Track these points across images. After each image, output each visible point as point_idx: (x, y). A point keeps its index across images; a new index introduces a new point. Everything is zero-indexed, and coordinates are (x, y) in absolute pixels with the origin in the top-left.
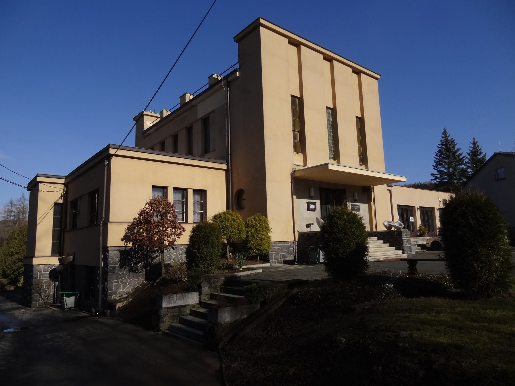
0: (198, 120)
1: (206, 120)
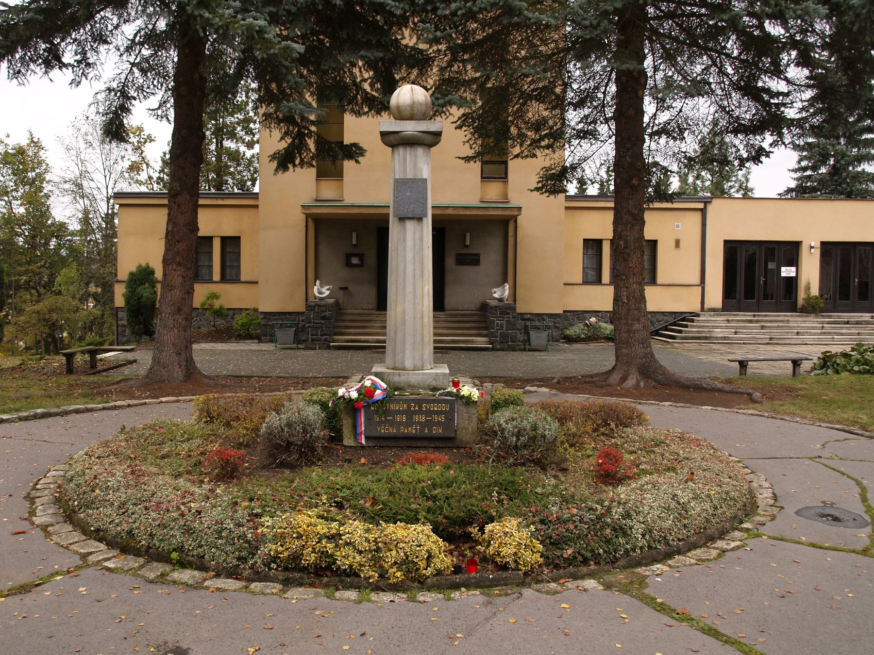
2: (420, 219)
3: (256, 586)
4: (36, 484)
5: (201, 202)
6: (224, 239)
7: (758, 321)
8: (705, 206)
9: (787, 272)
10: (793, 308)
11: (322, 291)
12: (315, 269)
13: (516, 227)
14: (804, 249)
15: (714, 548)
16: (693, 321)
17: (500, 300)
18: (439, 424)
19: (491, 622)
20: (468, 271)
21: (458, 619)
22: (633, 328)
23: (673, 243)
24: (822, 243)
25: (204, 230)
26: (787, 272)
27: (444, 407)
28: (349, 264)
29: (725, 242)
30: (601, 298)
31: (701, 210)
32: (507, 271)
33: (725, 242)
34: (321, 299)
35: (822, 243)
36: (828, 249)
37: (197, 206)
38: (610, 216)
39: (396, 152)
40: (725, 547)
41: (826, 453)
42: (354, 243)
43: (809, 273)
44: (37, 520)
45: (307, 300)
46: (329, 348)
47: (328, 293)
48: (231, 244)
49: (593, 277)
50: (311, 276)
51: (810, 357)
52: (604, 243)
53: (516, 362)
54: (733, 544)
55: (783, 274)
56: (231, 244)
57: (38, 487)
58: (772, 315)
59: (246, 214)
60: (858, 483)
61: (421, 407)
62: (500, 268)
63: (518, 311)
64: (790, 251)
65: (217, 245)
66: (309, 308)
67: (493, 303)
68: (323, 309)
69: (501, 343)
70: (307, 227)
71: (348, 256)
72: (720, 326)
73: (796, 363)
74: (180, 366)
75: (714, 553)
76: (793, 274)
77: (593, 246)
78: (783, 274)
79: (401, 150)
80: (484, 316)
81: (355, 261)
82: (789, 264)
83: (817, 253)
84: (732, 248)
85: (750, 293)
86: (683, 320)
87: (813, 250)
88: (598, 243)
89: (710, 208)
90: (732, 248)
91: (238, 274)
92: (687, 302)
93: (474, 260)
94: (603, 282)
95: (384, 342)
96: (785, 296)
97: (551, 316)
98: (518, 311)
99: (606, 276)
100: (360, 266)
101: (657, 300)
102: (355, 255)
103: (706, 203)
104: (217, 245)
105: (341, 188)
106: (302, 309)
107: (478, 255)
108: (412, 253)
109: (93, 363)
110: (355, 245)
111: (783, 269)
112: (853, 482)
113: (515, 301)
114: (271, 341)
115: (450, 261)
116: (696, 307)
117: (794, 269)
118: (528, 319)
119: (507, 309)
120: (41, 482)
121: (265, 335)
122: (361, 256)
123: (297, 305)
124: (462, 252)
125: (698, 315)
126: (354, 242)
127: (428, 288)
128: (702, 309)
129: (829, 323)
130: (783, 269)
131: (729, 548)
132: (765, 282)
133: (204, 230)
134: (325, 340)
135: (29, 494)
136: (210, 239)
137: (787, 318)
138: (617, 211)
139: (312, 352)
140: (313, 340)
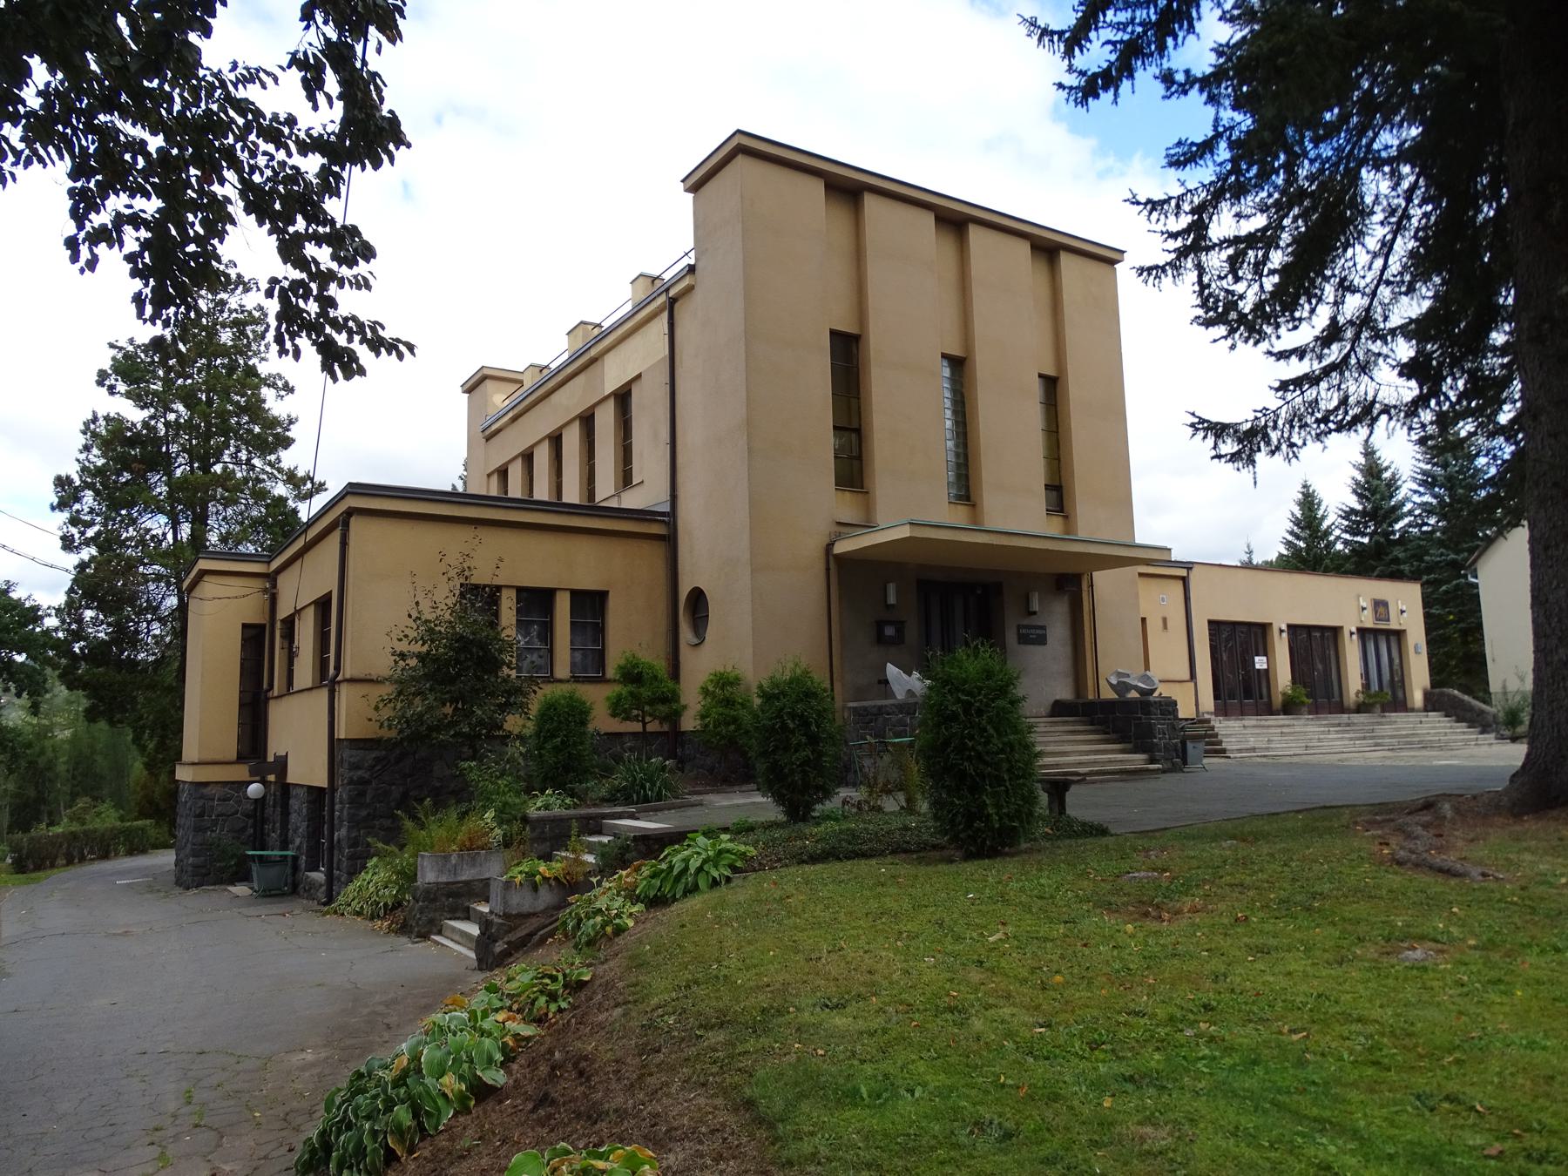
0: (515, 458)
1: (623, 397)
6: (576, 595)
28: (880, 639)
33: (245, 626)
65: (563, 605)
70: (828, 569)
71: (880, 625)
81: (889, 631)
90: (1215, 626)
93: (1042, 640)
102: (890, 623)
104: (563, 605)
107: (1043, 628)
124: (1026, 622)
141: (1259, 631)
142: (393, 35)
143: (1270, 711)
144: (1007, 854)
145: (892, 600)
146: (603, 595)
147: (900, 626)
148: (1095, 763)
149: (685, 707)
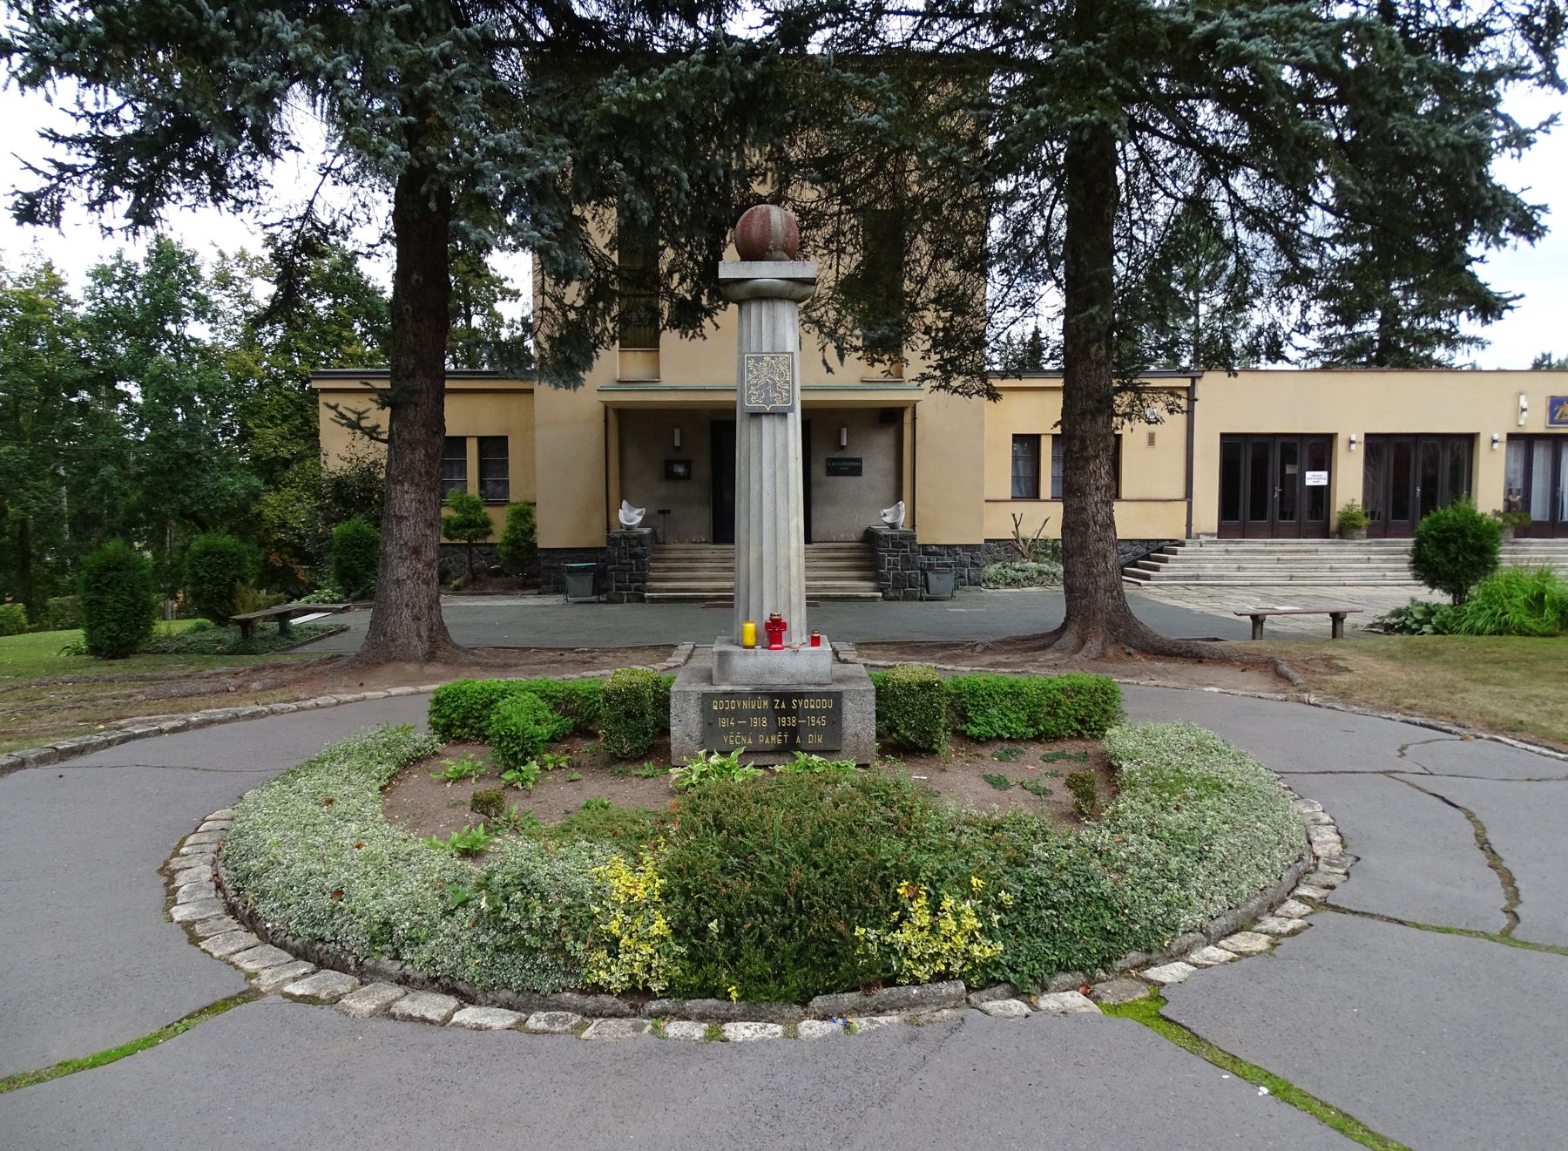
2: (784, 415)
3: (537, 1021)
4: (181, 844)
5: (449, 385)
6: (482, 440)
7: (1270, 552)
8: (1193, 383)
9: (1315, 478)
10: (1323, 530)
11: (630, 516)
12: (618, 484)
13: (914, 419)
14: (1341, 446)
15: (1260, 932)
16: (1175, 553)
17: (893, 526)
18: (818, 730)
19: (920, 1075)
20: (847, 483)
21: (867, 1070)
22: (1092, 563)
23: (1157, 440)
24: (1367, 435)
25: (453, 428)
26: (1315, 478)
27: (827, 704)
28: (670, 476)
29: (1223, 435)
30: (1044, 519)
31: (1187, 389)
32: (900, 486)
33: (1223, 435)
34: (629, 528)
35: (1367, 435)
36: (1376, 444)
37: (442, 393)
38: (1057, 401)
39: (745, 307)
40: (1279, 929)
41: (1405, 764)
42: (690, 454)
43: (1348, 484)
44: (179, 913)
45: (608, 529)
46: (642, 600)
47: (640, 519)
48: (494, 448)
49: (1027, 488)
50: (614, 494)
51: (1359, 607)
52: (1043, 439)
53: (911, 617)
54: (1290, 925)
55: (1308, 483)
56: (494, 448)
57: (183, 850)
58: (1292, 543)
59: (514, 402)
60: (1470, 816)
61: (789, 704)
62: (891, 480)
63: (919, 541)
64: (1320, 449)
65: (472, 449)
66: (612, 541)
67: (885, 531)
68: (634, 542)
69: (896, 588)
70: (606, 421)
71: (668, 464)
72: (1216, 558)
73: (1337, 618)
74: (419, 636)
75: (1261, 943)
76: (1324, 483)
77: (1027, 444)
78: (1308, 483)
79: (754, 308)
80: (872, 552)
81: (680, 470)
82: (1317, 467)
83: (1359, 450)
84: (1232, 445)
85: (1259, 511)
86: (1161, 551)
87: (1353, 447)
88: (1034, 440)
89: (1199, 385)
90: (1232, 445)
91: (506, 492)
92: (1165, 525)
93: (855, 469)
94: (1042, 496)
95: (732, 598)
96: (1313, 517)
97: (966, 547)
98: (919, 541)
99: (1046, 489)
100: (687, 477)
101: (1130, 522)
102: (679, 462)
103: (1193, 379)
104: (472, 449)
105: (657, 362)
106: (601, 542)
107: (860, 460)
108: (773, 463)
109: (285, 631)
110: (678, 448)
111: (1309, 474)
112: (1461, 814)
113: (914, 526)
114: (557, 591)
115: (819, 470)
116: (1179, 532)
117: (1325, 474)
118: (934, 554)
119: (903, 541)
120: (190, 840)
121: (548, 583)
122: (688, 464)
123: (594, 537)
124: (836, 455)
125: (1182, 544)
126: (677, 443)
127: (798, 521)
128: (1189, 536)
129: (1376, 553)
130: (1309, 474)
131: (1284, 930)
132: (1281, 494)
133: (453, 428)
134: (637, 589)
135: (167, 863)
136: (460, 442)
137: (1314, 547)
138: (1067, 391)
139: (617, 607)
140: (618, 589)
141: (1466, 444)
142: (65, 284)
143: (1324, 533)
144: (462, 665)
145: (677, 443)
146: (503, 440)
147: (688, 464)
148: (825, 588)
149: (1413, 600)
